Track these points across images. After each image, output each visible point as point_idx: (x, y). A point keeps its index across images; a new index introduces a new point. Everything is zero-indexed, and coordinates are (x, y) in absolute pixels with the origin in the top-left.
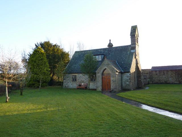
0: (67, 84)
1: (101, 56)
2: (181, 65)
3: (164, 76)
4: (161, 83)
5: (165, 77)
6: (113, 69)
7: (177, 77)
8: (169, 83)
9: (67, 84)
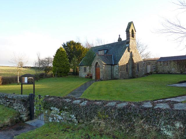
0: (81, 74)
1: (103, 51)
2: (185, 55)
3: (167, 66)
4: (165, 73)
5: (168, 68)
6: (101, 62)
7: (179, 67)
8: (171, 74)
9: (81, 74)
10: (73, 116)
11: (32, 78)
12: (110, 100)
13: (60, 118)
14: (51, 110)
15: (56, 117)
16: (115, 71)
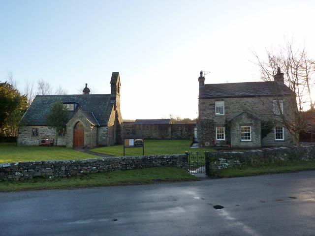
1: (73, 105)
10: (238, 161)
11: (142, 140)
12: (99, 183)
13: (227, 164)
14: (219, 161)
15: (224, 165)
16: (100, 135)
